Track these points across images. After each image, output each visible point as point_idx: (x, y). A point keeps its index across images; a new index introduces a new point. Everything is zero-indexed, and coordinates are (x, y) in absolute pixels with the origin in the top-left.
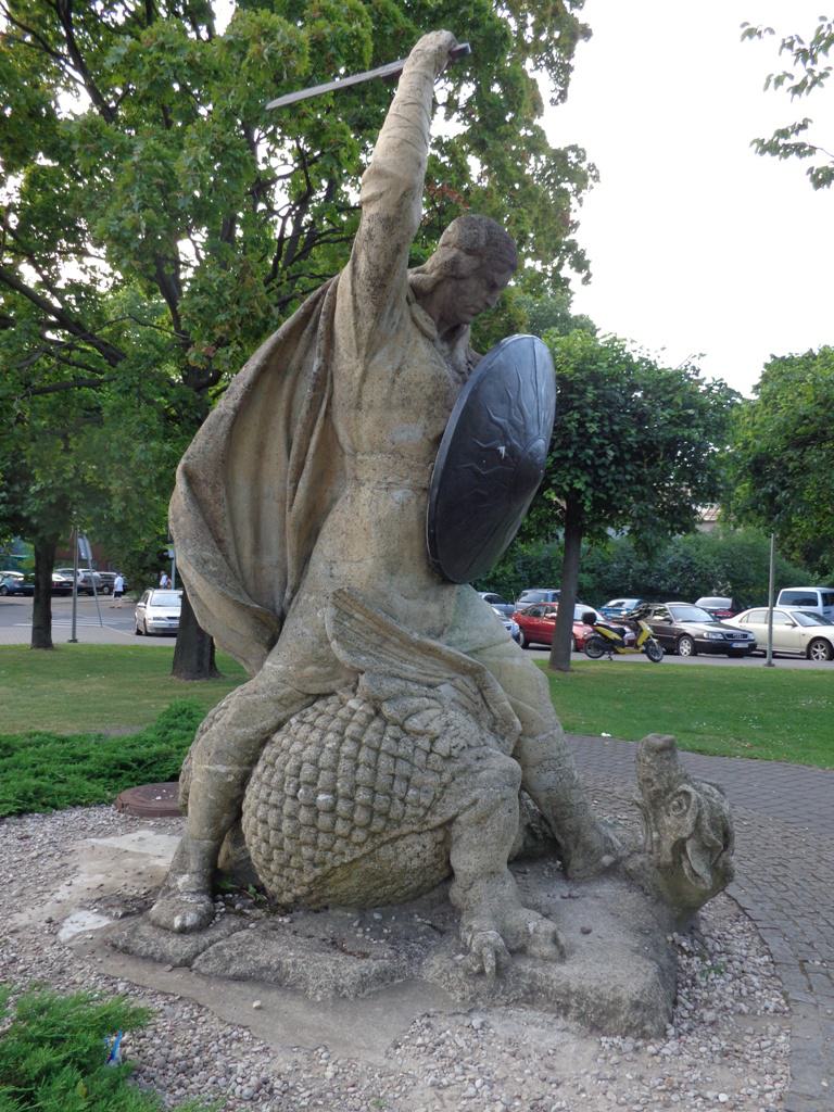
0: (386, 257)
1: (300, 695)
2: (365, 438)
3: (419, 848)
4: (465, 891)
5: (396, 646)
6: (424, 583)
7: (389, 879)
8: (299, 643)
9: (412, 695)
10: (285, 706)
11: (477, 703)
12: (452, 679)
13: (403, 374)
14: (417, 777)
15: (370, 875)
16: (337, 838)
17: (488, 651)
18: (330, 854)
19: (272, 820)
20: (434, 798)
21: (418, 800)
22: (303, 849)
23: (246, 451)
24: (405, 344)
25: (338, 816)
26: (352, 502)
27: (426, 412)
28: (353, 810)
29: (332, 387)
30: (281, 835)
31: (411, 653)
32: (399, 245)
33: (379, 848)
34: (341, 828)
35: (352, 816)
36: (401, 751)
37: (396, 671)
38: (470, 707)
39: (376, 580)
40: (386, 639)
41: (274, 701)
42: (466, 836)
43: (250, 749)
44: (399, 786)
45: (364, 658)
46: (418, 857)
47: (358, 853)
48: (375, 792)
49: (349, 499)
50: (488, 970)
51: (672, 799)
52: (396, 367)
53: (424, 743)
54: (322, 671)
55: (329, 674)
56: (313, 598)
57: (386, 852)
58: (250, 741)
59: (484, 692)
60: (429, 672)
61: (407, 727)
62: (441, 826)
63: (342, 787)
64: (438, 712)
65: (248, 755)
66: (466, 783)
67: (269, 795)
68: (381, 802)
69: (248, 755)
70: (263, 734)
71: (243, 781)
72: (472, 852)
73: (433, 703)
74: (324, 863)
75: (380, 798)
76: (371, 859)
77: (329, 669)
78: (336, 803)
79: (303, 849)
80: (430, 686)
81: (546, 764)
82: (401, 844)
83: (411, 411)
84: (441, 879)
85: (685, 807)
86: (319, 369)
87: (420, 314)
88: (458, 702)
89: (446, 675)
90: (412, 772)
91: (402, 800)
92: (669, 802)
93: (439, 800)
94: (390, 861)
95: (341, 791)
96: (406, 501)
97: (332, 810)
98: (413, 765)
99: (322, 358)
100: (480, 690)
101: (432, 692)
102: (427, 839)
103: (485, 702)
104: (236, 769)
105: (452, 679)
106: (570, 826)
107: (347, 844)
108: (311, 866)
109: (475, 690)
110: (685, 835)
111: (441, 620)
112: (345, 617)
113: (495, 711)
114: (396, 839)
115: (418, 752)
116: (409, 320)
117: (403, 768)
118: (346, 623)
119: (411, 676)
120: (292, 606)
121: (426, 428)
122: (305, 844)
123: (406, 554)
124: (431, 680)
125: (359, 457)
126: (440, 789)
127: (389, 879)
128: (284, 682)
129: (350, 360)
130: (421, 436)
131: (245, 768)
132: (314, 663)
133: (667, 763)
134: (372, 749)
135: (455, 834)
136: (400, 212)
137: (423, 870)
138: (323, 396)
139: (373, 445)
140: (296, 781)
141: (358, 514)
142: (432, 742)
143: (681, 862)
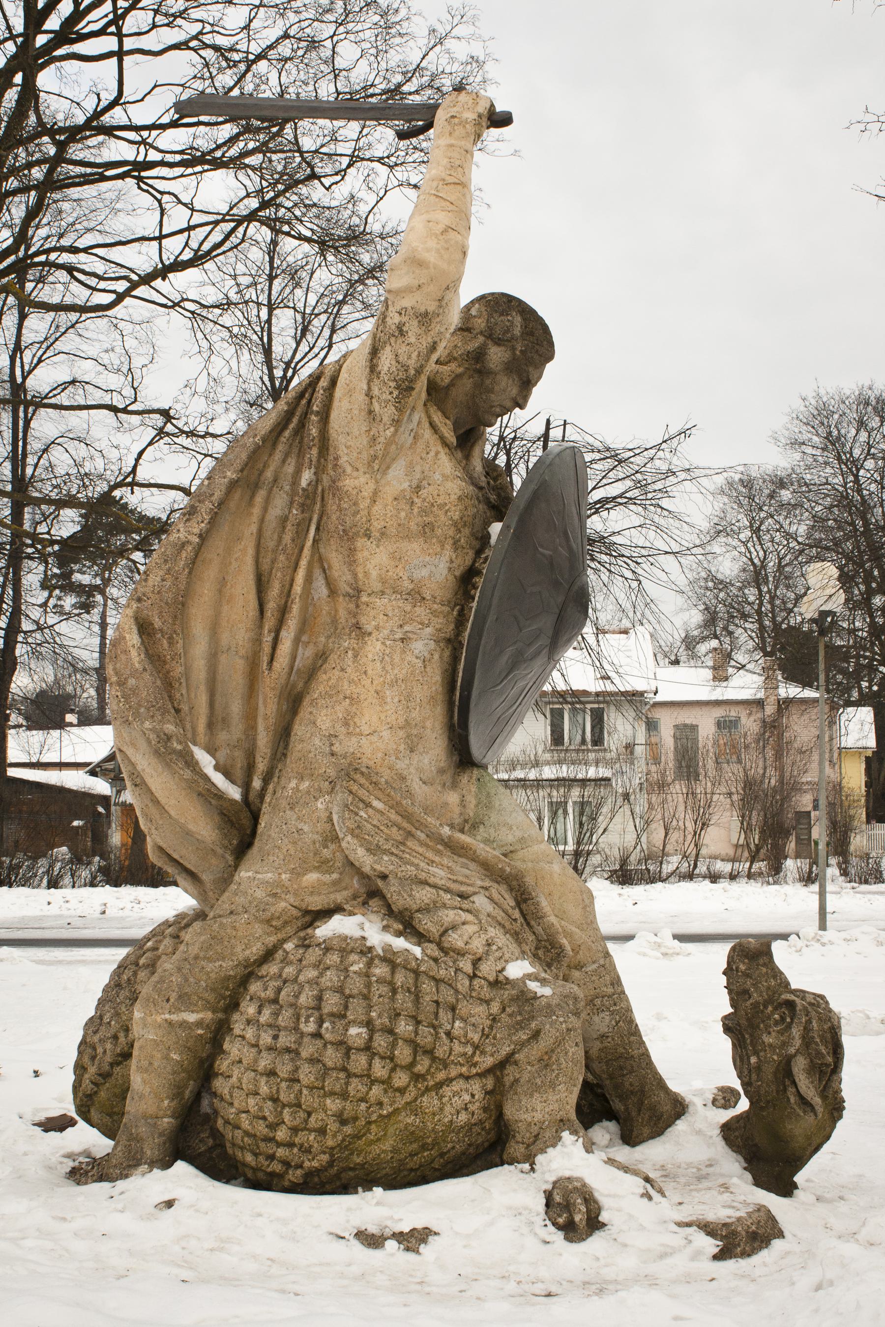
0: (419, 355)
1: (295, 912)
2: (374, 574)
3: (467, 1097)
4: (528, 1146)
5: (422, 844)
6: (442, 764)
7: (429, 1140)
8: (295, 843)
9: (444, 906)
10: (276, 928)
11: (515, 920)
12: (486, 889)
13: (423, 493)
14: (464, 1008)
15: (411, 1135)
16: (373, 1082)
17: (520, 854)
18: (363, 1106)
19: (284, 1070)
20: (483, 1034)
21: (466, 1036)
22: (328, 1101)
23: (206, 590)
24: (424, 455)
25: (374, 1054)
26: (355, 656)
27: (451, 541)
28: (394, 1045)
29: (323, 505)
30: (297, 1087)
31: (439, 853)
32: (435, 343)
33: (422, 1095)
34: (379, 1069)
35: (392, 1053)
36: (442, 972)
37: (423, 876)
38: (507, 924)
39: (393, 758)
40: (410, 834)
41: (262, 922)
42: (526, 1077)
43: (227, 989)
44: (445, 1016)
45: (386, 858)
46: (466, 1109)
47: (401, 1101)
48: (418, 1023)
49: (350, 652)
50: (577, 1218)
51: (773, 1013)
52: (415, 483)
53: (466, 965)
54: (327, 878)
55: (335, 883)
56: (307, 784)
57: (429, 1102)
58: (228, 978)
59: (524, 906)
60: (460, 878)
61: (446, 945)
62: (490, 1071)
63: (379, 1018)
64: (475, 928)
65: (224, 998)
66: (520, 1014)
67: (275, 1037)
68: (425, 1036)
69: (224, 998)
70: (245, 967)
71: (219, 1032)
72: (536, 1095)
73: (469, 917)
74: (355, 1119)
75: (424, 1030)
76: (412, 1111)
77: (335, 876)
78: (371, 1039)
79: (328, 1101)
80: (463, 896)
81: (598, 1002)
82: (447, 1091)
83: (434, 540)
84: (486, 1144)
85: (788, 1020)
86: (309, 485)
87: (437, 417)
88: (494, 918)
89: (479, 883)
90: (457, 1000)
91: (448, 1033)
92: (769, 1018)
93: (487, 1037)
94: (434, 1114)
95: (378, 1022)
96: (428, 656)
97: (367, 1048)
98: (457, 991)
99: (313, 470)
100: (518, 904)
101: (465, 905)
102: (476, 1086)
103: (525, 919)
104: (208, 1016)
105: (486, 889)
106: (631, 1085)
107: (386, 1091)
108: (337, 1125)
109: (513, 903)
110: (792, 1050)
111: (461, 814)
112: (361, 805)
113: (539, 930)
114: (439, 1085)
115: (460, 976)
116: (427, 425)
117: (447, 995)
118: (362, 813)
119: (440, 883)
120: (268, 799)
121: (452, 561)
122: (332, 1094)
123: (428, 724)
124: (463, 888)
125: (364, 599)
126: (489, 1022)
127: (429, 1140)
128: (275, 895)
129: (355, 474)
130: (445, 572)
131: (220, 1015)
132: (317, 869)
133: (764, 970)
134: (410, 970)
135: (508, 1080)
136: (440, 307)
137: (470, 1126)
138: (310, 520)
139: (384, 582)
140: (316, 1014)
141: (365, 673)
142: (476, 962)
143: (785, 1090)
